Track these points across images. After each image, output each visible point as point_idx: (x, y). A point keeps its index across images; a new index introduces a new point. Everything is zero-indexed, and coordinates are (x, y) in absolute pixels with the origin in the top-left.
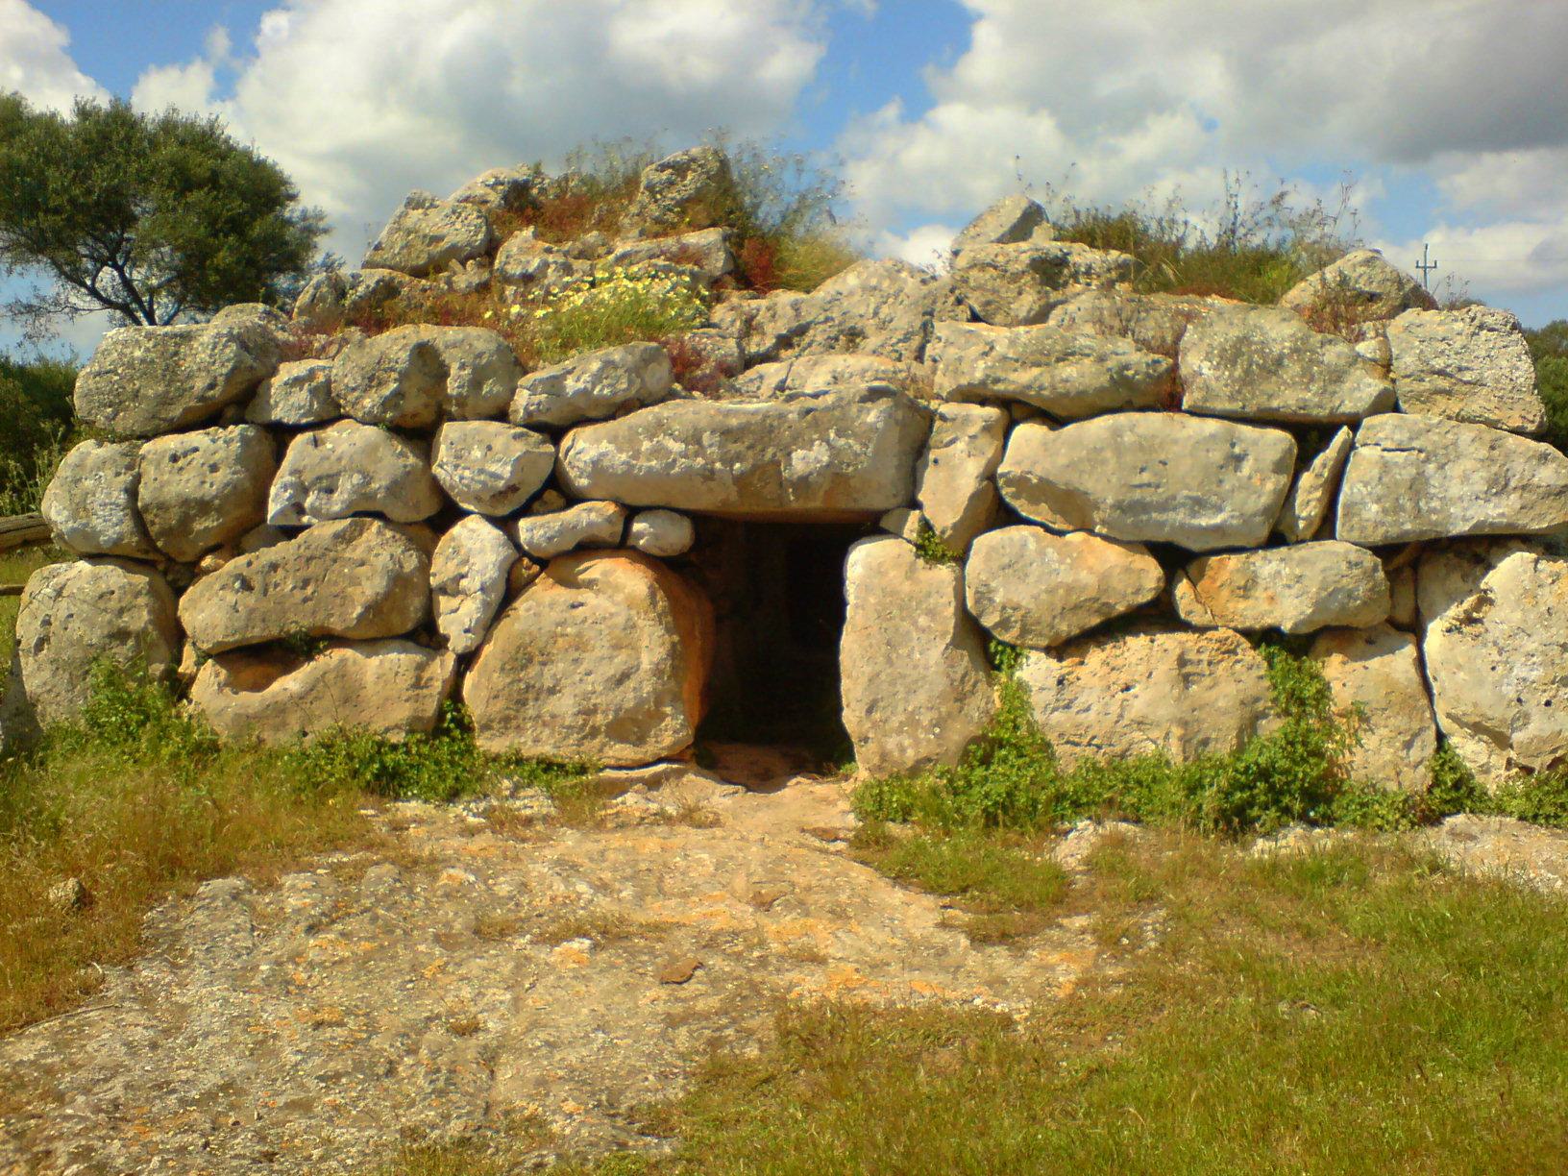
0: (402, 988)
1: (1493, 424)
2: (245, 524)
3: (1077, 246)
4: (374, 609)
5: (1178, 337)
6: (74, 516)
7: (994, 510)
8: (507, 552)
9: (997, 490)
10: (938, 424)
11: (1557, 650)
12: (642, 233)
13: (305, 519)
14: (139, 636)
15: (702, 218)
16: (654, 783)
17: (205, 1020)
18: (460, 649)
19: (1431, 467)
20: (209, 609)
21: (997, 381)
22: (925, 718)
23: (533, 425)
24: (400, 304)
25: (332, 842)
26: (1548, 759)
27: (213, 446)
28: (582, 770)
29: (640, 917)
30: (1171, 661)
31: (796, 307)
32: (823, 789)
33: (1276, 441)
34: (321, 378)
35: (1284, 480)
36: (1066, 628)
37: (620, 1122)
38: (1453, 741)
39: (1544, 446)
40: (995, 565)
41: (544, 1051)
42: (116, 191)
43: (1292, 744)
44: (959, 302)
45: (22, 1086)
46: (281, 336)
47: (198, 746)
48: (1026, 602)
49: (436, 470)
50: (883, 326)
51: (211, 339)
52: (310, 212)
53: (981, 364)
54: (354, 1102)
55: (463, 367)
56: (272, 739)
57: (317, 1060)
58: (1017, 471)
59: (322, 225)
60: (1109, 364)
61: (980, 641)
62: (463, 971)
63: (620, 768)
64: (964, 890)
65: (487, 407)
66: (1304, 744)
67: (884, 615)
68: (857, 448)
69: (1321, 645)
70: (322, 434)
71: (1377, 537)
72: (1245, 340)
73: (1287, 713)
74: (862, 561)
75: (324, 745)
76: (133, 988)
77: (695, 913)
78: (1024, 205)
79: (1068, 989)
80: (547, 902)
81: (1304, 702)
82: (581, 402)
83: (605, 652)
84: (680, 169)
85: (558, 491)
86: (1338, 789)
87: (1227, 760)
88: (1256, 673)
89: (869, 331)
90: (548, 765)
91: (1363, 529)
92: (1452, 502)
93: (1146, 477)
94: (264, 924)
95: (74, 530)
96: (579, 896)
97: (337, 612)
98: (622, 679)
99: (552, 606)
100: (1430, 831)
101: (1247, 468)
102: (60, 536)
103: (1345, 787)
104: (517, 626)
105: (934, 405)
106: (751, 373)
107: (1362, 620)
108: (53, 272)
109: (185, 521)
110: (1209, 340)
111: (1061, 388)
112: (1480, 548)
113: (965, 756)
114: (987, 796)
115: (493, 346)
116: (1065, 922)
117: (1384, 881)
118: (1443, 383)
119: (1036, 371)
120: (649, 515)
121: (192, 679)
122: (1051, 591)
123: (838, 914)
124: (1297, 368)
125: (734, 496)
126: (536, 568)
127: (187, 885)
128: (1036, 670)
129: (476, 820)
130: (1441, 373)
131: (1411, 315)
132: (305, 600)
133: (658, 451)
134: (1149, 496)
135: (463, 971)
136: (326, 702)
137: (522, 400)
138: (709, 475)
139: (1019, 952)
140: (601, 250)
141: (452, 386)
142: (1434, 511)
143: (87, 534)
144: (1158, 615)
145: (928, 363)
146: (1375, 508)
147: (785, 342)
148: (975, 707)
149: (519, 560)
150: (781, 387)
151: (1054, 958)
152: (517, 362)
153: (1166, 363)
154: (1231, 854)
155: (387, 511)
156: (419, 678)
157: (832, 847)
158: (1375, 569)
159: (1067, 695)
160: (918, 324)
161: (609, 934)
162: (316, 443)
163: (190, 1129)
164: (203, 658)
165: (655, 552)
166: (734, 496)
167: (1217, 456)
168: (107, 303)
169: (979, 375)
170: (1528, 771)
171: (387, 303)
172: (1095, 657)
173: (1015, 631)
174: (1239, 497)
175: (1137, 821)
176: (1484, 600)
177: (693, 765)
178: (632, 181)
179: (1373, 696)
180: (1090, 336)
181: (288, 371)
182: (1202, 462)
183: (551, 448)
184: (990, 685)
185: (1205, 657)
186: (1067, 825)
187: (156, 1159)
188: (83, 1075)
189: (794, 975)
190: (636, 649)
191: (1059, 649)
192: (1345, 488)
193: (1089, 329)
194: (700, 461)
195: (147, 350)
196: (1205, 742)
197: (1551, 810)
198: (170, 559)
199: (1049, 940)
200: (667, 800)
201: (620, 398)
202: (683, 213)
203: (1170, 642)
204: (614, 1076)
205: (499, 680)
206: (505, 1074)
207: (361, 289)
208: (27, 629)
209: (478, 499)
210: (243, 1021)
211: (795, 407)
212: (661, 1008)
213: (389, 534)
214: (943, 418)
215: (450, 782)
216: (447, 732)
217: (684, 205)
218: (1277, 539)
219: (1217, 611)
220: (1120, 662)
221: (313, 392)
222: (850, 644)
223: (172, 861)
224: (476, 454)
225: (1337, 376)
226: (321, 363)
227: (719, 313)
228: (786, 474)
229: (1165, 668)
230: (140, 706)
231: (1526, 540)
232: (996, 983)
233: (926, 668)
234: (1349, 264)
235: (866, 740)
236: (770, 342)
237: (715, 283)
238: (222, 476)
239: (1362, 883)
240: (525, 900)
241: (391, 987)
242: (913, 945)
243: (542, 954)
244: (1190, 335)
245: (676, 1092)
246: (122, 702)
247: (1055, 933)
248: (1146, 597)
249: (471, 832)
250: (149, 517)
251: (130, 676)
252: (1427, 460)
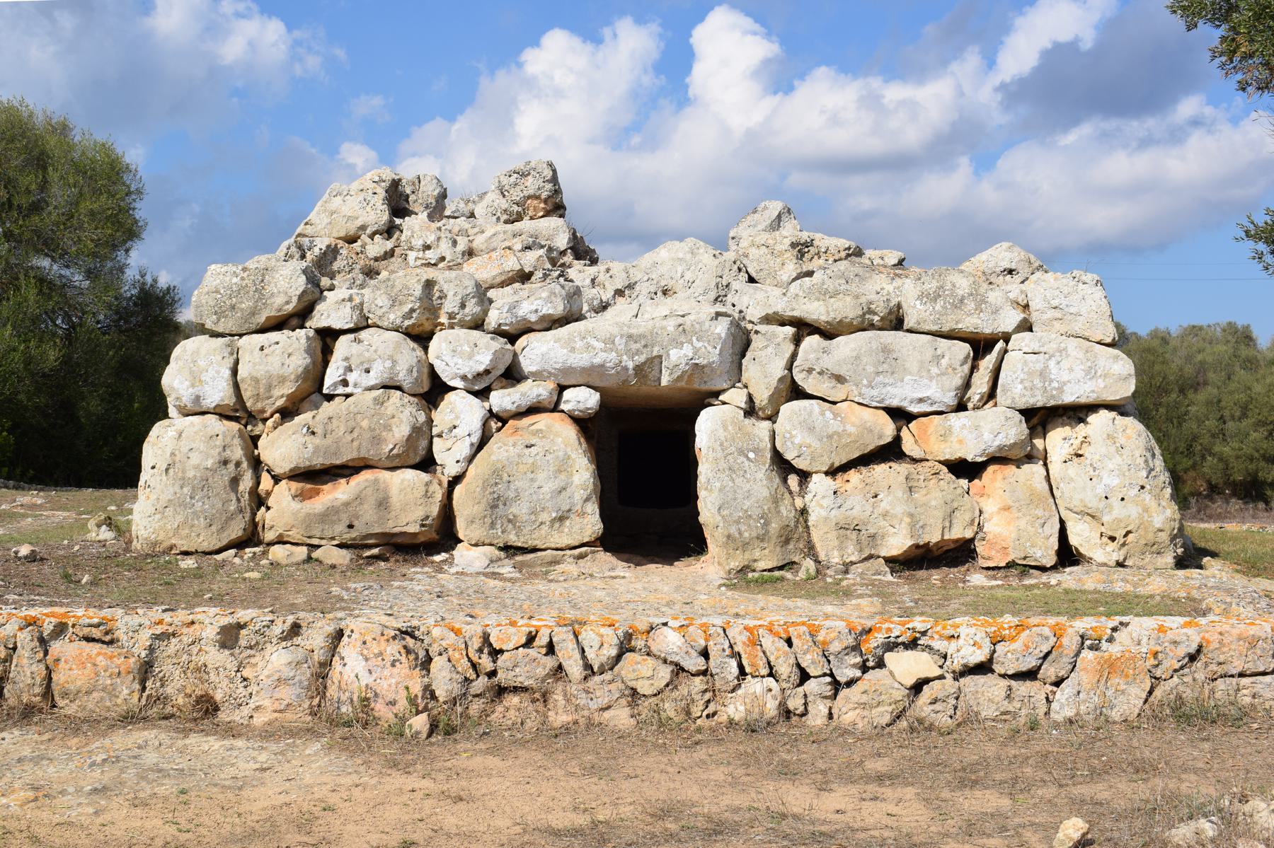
2: (311, 390)
16: (581, 557)
23: (499, 333)
30: (902, 479)
63: (557, 549)
71: (1022, 404)
85: (512, 375)
105: (749, 326)
112: (1077, 413)
118: (1058, 314)
121: (269, 494)
144: (891, 452)
146: (1020, 386)
170: (1113, 539)
172: (853, 475)
182: (924, 374)
183: (509, 346)
191: (832, 472)
192: (1002, 375)
195: (243, 279)
214: (757, 332)
218: (961, 407)
221: (353, 308)
248: (889, 439)
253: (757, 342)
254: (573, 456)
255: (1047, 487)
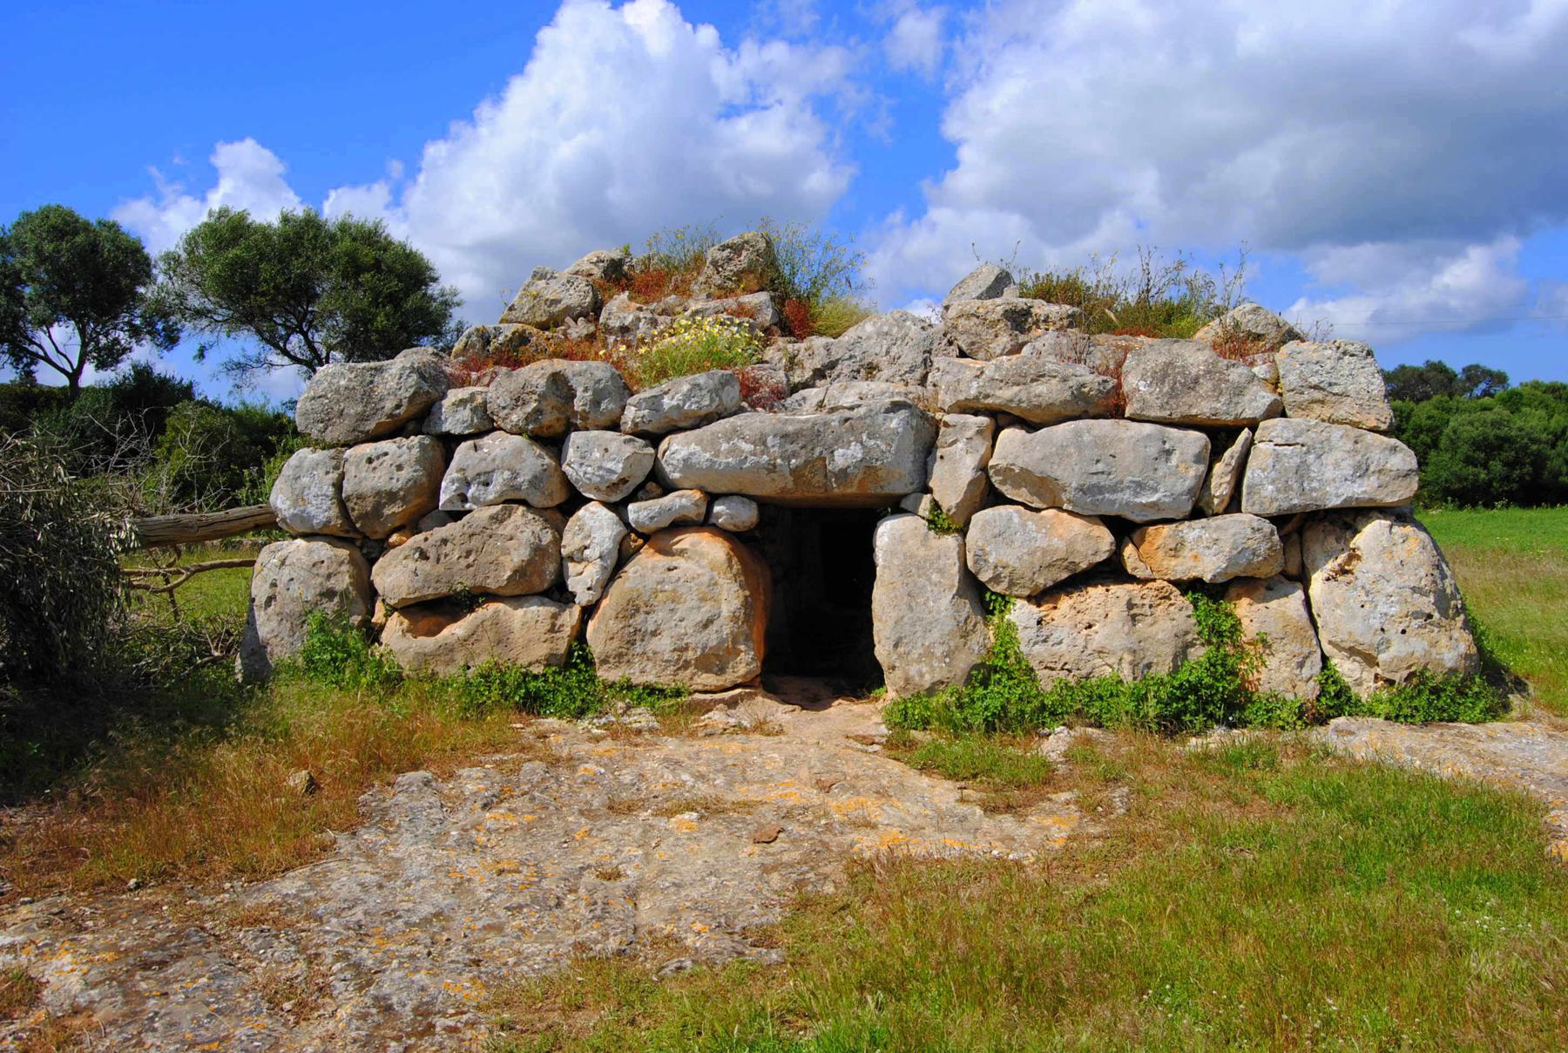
0: (559, 847)
1: (1356, 425)
2: (423, 509)
3: (1038, 302)
4: (520, 573)
5: (1120, 365)
6: (295, 504)
7: (987, 494)
8: (619, 529)
9: (988, 478)
10: (943, 429)
11: (1408, 592)
12: (709, 296)
13: (468, 506)
14: (344, 595)
15: (754, 284)
16: (732, 704)
17: (415, 869)
18: (584, 603)
19: (1311, 457)
20: (396, 574)
21: (987, 396)
22: (939, 651)
24: (530, 348)
25: (495, 746)
26: (1405, 673)
27: (399, 452)
28: (678, 693)
29: (730, 797)
31: (828, 348)
32: (858, 708)
33: (1196, 440)
34: (479, 400)
35: (1202, 468)
36: (1043, 580)
37: (736, 937)
38: (1333, 661)
39: (1393, 441)
40: (988, 535)
41: (673, 889)
42: (303, 276)
43: (1213, 665)
44: (950, 343)
45: (290, 911)
46: (448, 370)
47: (388, 678)
48: (1012, 561)
49: (565, 468)
50: (894, 361)
51: (397, 376)
52: (447, 290)
53: (975, 384)
54: (535, 925)
55: (586, 390)
56: (443, 671)
57: (504, 897)
58: (1003, 464)
59: (456, 299)
60: (1070, 383)
61: (978, 593)
62: (604, 835)
63: (706, 692)
64: (975, 776)
65: (603, 420)
66: (1223, 665)
67: (905, 573)
68: (883, 447)
69: (1233, 591)
70: (479, 442)
71: (1273, 509)
72: (1169, 364)
73: (1209, 642)
74: (887, 533)
75: (482, 676)
76: (358, 847)
77: (773, 795)
78: (997, 272)
79: (1062, 843)
80: (660, 787)
81: (1221, 634)
82: (675, 416)
83: (695, 603)
84: (737, 249)
85: (657, 482)
86: (1249, 700)
87: (1166, 679)
88: (1185, 613)
89: (882, 366)
90: (652, 690)
91: (1262, 504)
92: (1328, 483)
93: (1100, 467)
94: (451, 804)
95: (294, 515)
96: (684, 782)
97: (492, 575)
98: (707, 624)
99: (653, 569)
100: (1321, 729)
101: (1174, 459)
102: (284, 520)
103: (1255, 698)
104: (627, 585)
105: (938, 416)
106: (796, 396)
107: (1264, 572)
108: (257, 338)
109: (378, 508)
110: (1142, 368)
111: (1035, 401)
112: (1349, 518)
113: (969, 680)
114: (986, 708)
115: (608, 374)
116: (1053, 796)
117: (1288, 764)
118: (1318, 395)
119: (1016, 389)
120: (727, 501)
121: (382, 627)
122: (1032, 554)
123: (882, 793)
124: (1210, 385)
125: (790, 485)
126: (640, 541)
127: (391, 777)
128: (1021, 613)
129: (599, 731)
130: (1316, 387)
131: (1292, 345)
132: (468, 566)
133: (733, 451)
134: (1102, 480)
135: (604, 835)
136: (485, 643)
137: (630, 414)
138: (772, 468)
139: (1022, 819)
140: (679, 309)
141: (578, 405)
142: (1313, 490)
143: (303, 518)
144: (1111, 571)
145: (930, 387)
146: (1270, 487)
147: (820, 374)
148: (975, 640)
149: (628, 535)
150: (820, 405)
151: (1048, 822)
152: (626, 387)
153: (1112, 382)
154: (1173, 748)
155: (529, 499)
156: (553, 625)
157: (870, 749)
158: (1272, 534)
159: (1045, 632)
160: (920, 359)
161: (710, 809)
162: (476, 448)
163: (416, 942)
164: (393, 609)
165: (731, 527)
166: (790, 485)
167: (1153, 451)
168: (295, 360)
169: (973, 392)
170: (1391, 682)
171: (522, 348)
172: (1065, 603)
173: (1004, 585)
174: (1169, 481)
175: (1100, 726)
176: (1354, 556)
177: (760, 690)
178: (699, 260)
179: (1274, 630)
180: (1050, 364)
181: (454, 395)
182: (1144, 459)
183: (651, 450)
184: (986, 625)
185: (1147, 602)
186: (1047, 730)
187: (395, 962)
188: (333, 905)
189: (855, 836)
190: (717, 601)
191: (1040, 597)
192: (1248, 473)
193: (1051, 358)
194: (765, 457)
196: (1149, 666)
197: (1407, 711)
198: (365, 537)
199: (1043, 810)
200: (744, 714)
201: (703, 412)
202: (739, 281)
203: (1121, 591)
204: (728, 906)
205: (614, 626)
206: (644, 906)
207: (501, 338)
208: (260, 590)
209: (598, 489)
210: (445, 869)
211: (836, 416)
212: (756, 859)
213: (531, 516)
214: (946, 425)
215: (578, 703)
216: (575, 666)
217: (740, 275)
218: (1197, 513)
219: (1155, 567)
220: (1083, 606)
221: (474, 410)
222: (879, 595)
223: (380, 759)
224: (595, 455)
225: (1239, 391)
226: (478, 389)
227: (770, 353)
228: (830, 467)
229: (1118, 611)
230: (344, 645)
231: (1383, 511)
232: (1008, 839)
233: (939, 612)
234: (1239, 313)
235: (894, 668)
236: (808, 374)
237: (766, 330)
238: (406, 474)
239: (1272, 765)
240: (643, 786)
241: (551, 846)
242: (941, 815)
243: (662, 822)
244: (1130, 362)
245: (776, 916)
246: (330, 643)
247: (1046, 805)
249: (597, 739)
250: (350, 505)
251: (336, 625)
252: (1308, 452)
253: (945, 435)
254: (721, 581)
255: (1305, 615)
